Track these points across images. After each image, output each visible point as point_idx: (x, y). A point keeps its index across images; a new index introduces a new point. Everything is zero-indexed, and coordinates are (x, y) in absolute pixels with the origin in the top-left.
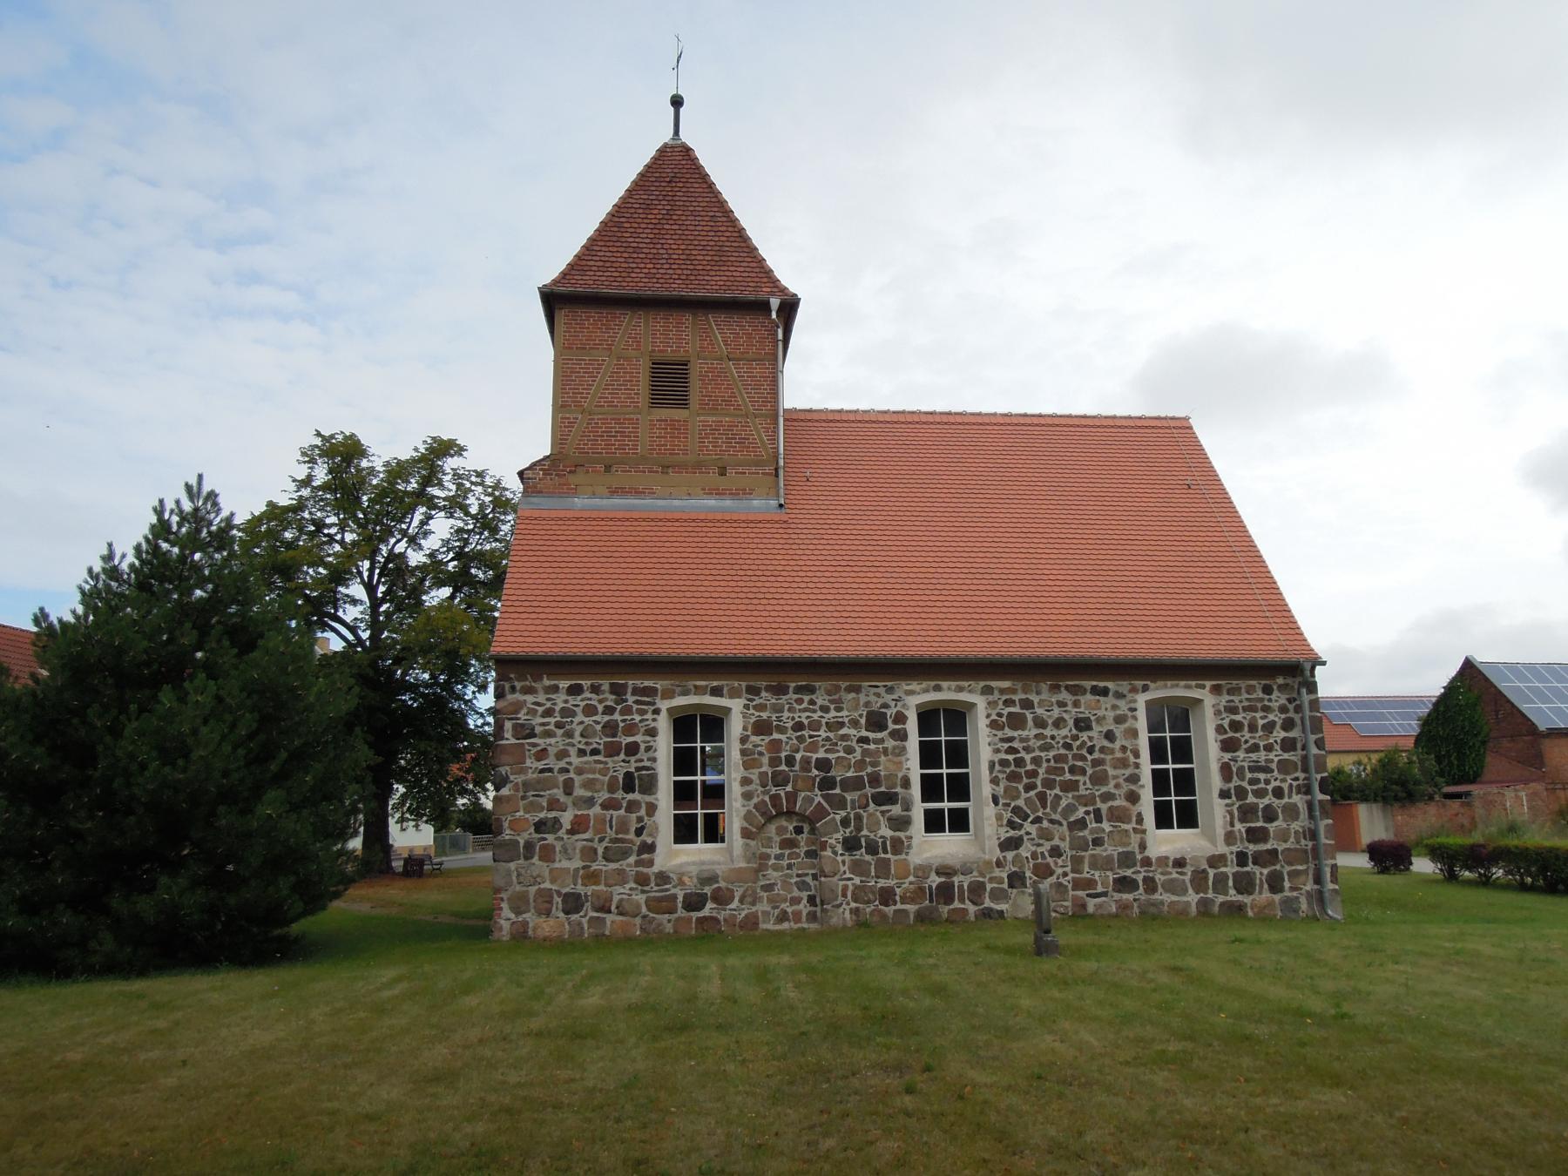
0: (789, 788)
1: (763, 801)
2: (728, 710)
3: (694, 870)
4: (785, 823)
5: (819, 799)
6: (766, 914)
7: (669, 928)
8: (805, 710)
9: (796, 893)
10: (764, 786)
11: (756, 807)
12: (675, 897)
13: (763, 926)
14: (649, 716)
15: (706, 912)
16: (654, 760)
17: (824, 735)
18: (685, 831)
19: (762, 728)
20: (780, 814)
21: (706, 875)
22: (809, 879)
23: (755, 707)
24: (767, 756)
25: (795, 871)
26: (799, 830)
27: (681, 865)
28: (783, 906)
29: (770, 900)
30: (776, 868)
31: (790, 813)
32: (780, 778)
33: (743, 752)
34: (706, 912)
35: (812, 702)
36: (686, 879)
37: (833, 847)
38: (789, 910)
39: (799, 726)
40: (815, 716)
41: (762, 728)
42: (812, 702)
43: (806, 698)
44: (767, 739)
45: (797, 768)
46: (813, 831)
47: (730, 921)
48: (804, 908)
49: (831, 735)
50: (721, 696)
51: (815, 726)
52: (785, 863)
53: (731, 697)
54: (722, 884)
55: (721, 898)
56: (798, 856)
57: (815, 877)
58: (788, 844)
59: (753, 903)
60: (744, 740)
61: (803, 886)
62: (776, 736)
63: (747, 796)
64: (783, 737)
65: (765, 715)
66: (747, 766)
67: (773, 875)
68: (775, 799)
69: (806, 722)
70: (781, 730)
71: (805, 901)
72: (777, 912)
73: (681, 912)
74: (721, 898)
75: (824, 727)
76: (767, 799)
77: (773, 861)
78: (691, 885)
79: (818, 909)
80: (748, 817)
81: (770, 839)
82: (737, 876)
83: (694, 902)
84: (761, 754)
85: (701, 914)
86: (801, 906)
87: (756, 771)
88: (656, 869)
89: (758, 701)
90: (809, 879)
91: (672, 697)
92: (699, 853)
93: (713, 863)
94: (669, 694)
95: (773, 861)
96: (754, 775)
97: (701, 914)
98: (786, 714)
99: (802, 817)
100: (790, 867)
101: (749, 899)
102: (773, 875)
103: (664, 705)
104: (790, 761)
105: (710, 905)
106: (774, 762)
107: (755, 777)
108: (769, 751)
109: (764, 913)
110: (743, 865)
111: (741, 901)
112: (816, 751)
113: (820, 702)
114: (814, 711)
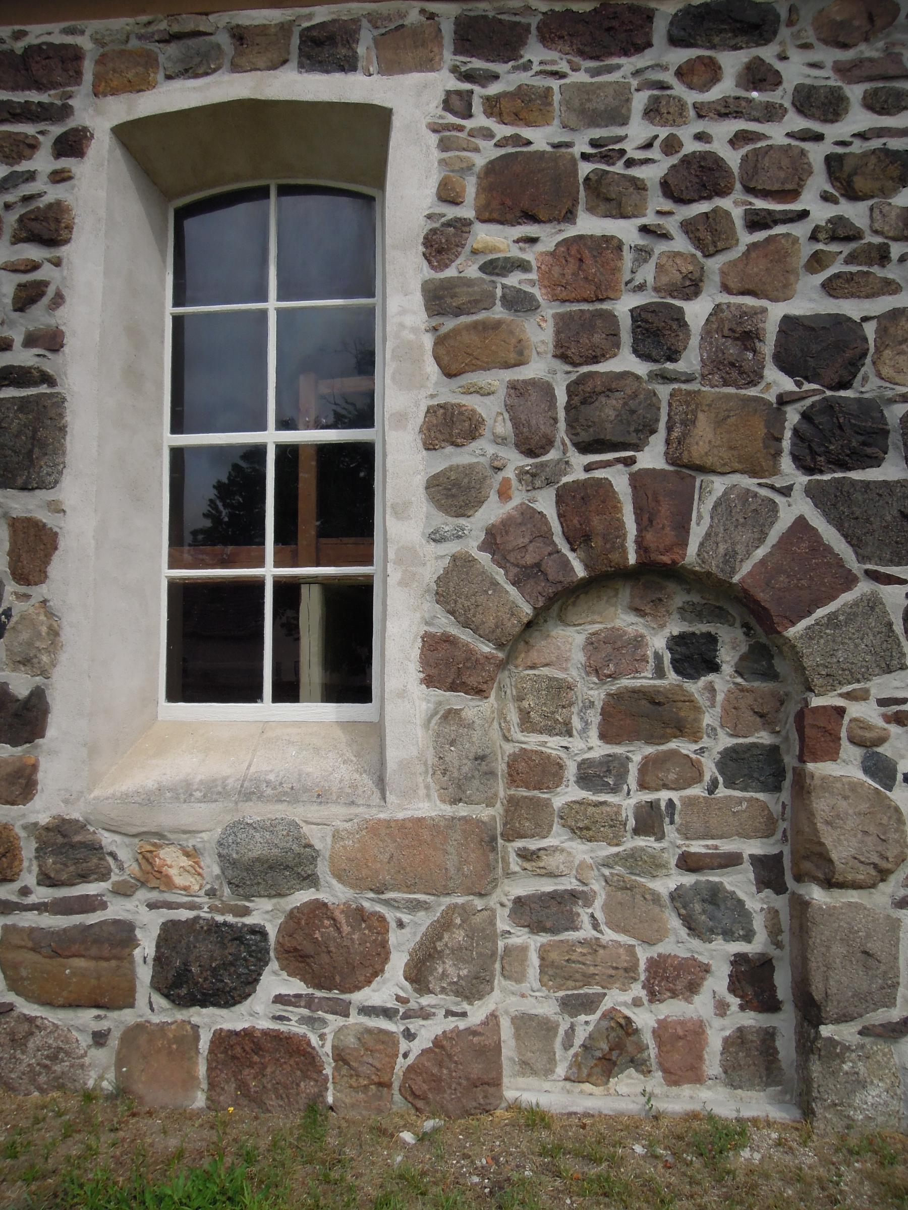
0: (652, 457)
1: (530, 517)
2: (378, 119)
3: (207, 822)
4: (626, 622)
5: (798, 507)
6: (533, 1029)
7: (99, 1070)
8: (727, 110)
9: (677, 943)
10: (532, 446)
11: (493, 541)
12: (122, 936)
13: (521, 1090)
14: (43, 162)
15: (255, 1014)
16: (52, 341)
17: (821, 213)
18: (213, 651)
19: (521, 191)
20: (605, 579)
21: (257, 847)
22: (739, 883)
23: (493, 106)
24: (550, 310)
25: (672, 842)
26: (694, 657)
27: (150, 799)
28: (617, 998)
29: (552, 972)
30: (584, 824)
31: (654, 577)
32: (608, 410)
33: (438, 299)
34: (255, 1014)
35: (759, 76)
36: (172, 860)
37: (868, 742)
38: (645, 1019)
39: (699, 177)
40: (776, 134)
41: (521, 191)
42: (759, 76)
43: (732, 62)
44: (550, 237)
45: (691, 361)
46: (762, 659)
47: (366, 1059)
48: (715, 1014)
49: (856, 213)
50: (348, 65)
51: (776, 178)
52: (628, 802)
53: (390, 68)
54: (334, 893)
55: (330, 957)
56: (691, 772)
57: (769, 873)
58: (639, 716)
59: (473, 988)
60: (440, 245)
61: (708, 912)
62: (588, 224)
63: (453, 494)
64: (625, 230)
65: (540, 138)
66: (453, 359)
67: (574, 857)
68: (584, 506)
69: (733, 158)
70: (610, 197)
71: (718, 982)
72: (586, 1025)
73: (150, 1008)
74: (330, 957)
75: (819, 181)
76: (546, 503)
77: (568, 793)
78: (194, 885)
79: (785, 1022)
80: (453, 589)
81: (559, 690)
82: (404, 856)
83: (206, 965)
84: (519, 302)
85: (233, 1019)
86: (700, 1007)
87: (497, 379)
88: (41, 809)
89: (509, 79)
90: (739, 883)
91: (140, 85)
92: (272, 745)
93: (290, 794)
94: (125, 71)
95: (568, 793)
96: (488, 398)
97: (233, 1019)
98: (637, 130)
99: (717, 595)
100: (649, 821)
101: (449, 968)
102: (574, 857)
103: (102, 117)
104: (657, 333)
105: (275, 981)
106: (580, 341)
107: (490, 409)
108: (558, 289)
109: (522, 1022)
110: (428, 807)
111: (418, 975)
112: (782, 293)
113: (795, 71)
114: (772, 113)
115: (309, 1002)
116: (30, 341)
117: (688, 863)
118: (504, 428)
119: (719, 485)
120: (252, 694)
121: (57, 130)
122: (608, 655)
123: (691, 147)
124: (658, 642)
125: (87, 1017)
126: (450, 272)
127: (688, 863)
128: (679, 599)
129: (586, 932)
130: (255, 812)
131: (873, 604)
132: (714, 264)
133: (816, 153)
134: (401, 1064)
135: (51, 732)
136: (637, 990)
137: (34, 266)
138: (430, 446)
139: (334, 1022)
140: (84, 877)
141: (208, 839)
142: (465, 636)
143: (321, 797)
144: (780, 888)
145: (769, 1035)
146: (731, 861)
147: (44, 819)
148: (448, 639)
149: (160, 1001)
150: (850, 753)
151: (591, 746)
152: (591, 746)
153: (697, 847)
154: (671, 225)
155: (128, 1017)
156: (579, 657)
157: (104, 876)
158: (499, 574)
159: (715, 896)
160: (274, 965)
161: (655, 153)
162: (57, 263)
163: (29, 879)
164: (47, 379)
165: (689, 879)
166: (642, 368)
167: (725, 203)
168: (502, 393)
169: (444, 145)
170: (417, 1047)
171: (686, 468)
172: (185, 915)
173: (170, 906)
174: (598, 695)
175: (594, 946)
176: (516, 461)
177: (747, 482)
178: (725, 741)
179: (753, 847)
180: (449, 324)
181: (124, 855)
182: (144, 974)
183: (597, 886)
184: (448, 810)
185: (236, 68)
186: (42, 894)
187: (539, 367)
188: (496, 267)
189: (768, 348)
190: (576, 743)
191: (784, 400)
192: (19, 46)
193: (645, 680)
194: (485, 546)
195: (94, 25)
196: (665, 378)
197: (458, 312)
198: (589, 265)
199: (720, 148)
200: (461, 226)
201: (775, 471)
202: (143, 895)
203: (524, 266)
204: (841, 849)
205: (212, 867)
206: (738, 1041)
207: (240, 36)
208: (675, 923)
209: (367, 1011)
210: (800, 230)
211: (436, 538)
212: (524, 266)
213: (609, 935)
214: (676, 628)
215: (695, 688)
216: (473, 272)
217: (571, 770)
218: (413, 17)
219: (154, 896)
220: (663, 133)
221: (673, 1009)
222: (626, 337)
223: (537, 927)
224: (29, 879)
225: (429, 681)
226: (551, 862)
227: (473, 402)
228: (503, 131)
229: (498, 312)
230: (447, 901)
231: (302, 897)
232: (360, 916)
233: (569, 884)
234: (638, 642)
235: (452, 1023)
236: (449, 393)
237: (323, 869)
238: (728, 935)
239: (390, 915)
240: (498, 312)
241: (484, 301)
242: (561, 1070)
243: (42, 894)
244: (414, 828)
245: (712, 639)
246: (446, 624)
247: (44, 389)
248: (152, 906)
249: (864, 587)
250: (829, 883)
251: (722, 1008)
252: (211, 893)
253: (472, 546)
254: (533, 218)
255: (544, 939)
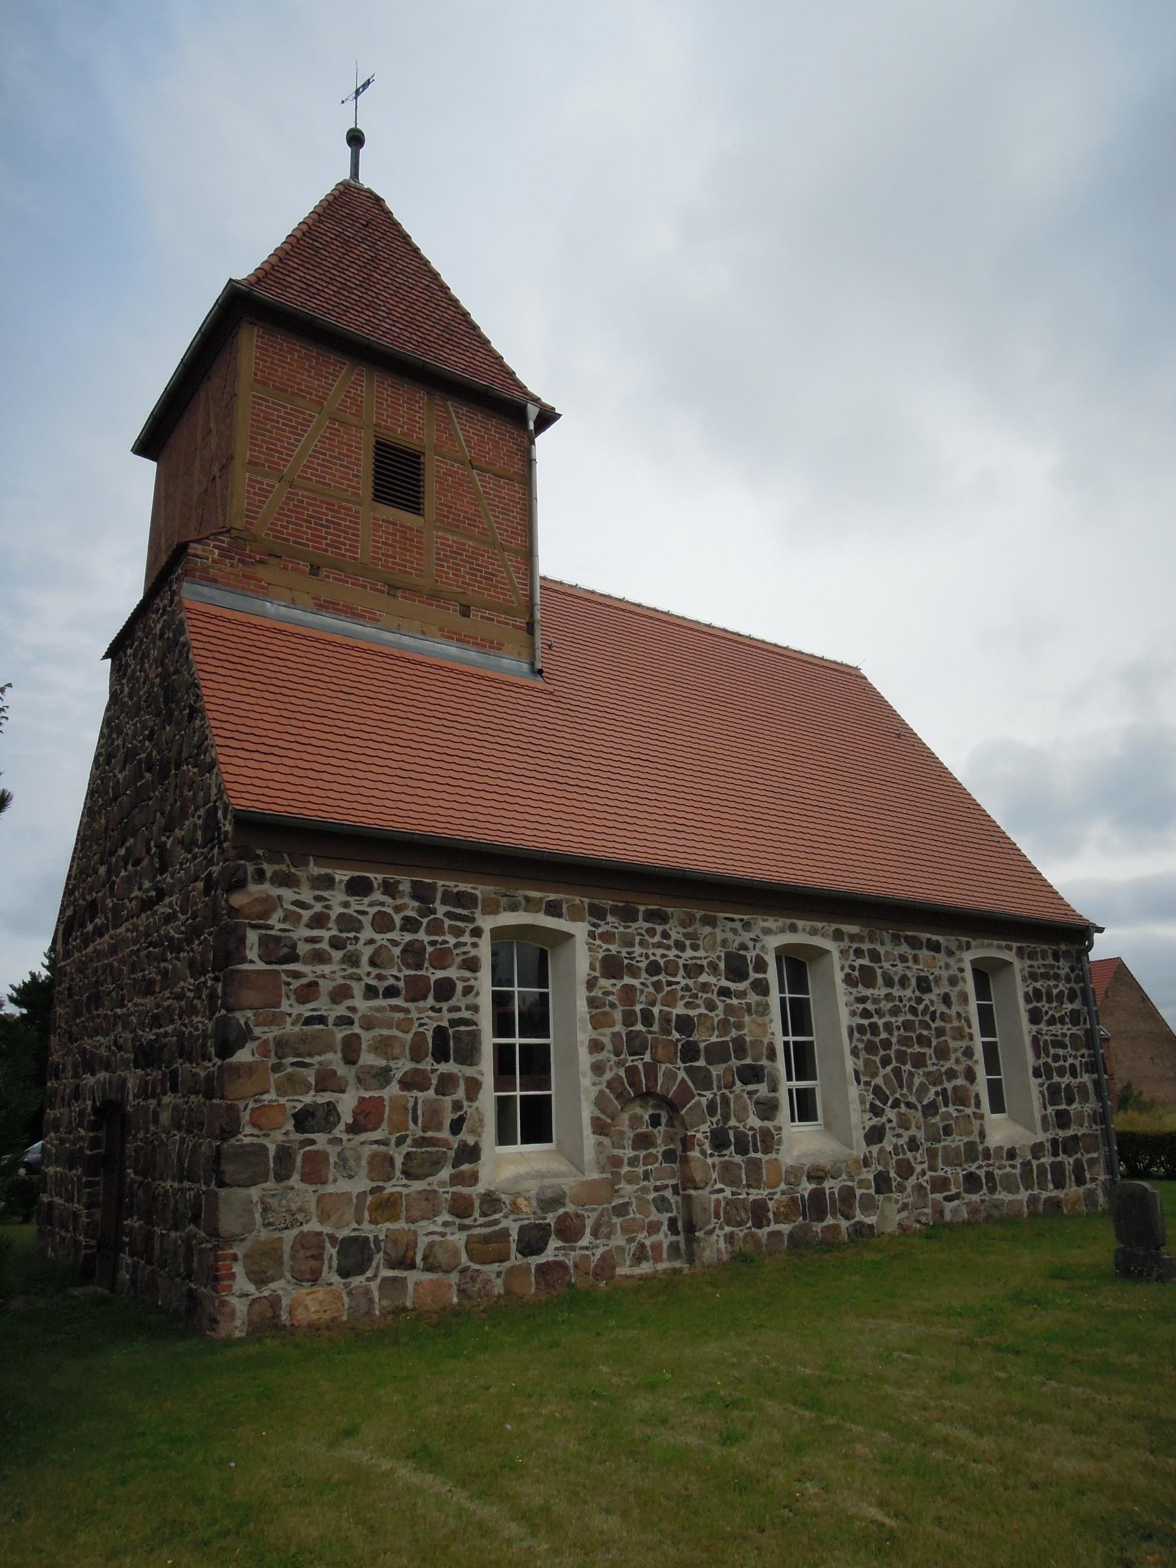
0: (647, 1058)
4: (638, 1111)
5: (682, 1074)
8: (659, 945)
9: (655, 1216)
11: (609, 1085)
12: (505, 1233)
15: (548, 1256)
17: (683, 982)
19: (612, 967)
21: (549, 1194)
22: (668, 1193)
25: (652, 1183)
26: (655, 1121)
29: (624, 1230)
33: (592, 1003)
34: (548, 1256)
36: (522, 1202)
43: (659, 929)
45: (656, 1027)
48: (664, 1237)
49: (690, 982)
52: (641, 1170)
54: (570, 1208)
55: (569, 1231)
60: (591, 984)
61: (662, 1204)
62: (628, 980)
63: (598, 1069)
69: (662, 962)
71: (665, 1228)
73: (515, 1259)
75: (681, 972)
76: (622, 1073)
79: (681, 1238)
82: (591, 1194)
83: (532, 1242)
86: (660, 1236)
87: (608, 1031)
88: (481, 1188)
90: (668, 1193)
93: (556, 1175)
94: (492, 908)
95: (625, 1169)
100: (646, 1175)
101: (604, 1230)
103: (488, 923)
104: (647, 1018)
105: (554, 1243)
107: (606, 1040)
111: (595, 1234)
113: (674, 936)
114: (668, 948)
115: (564, 1248)
116: (468, 1008)
117: (657, 1189)
118: (611, 1047)
119: (663, 1066)
120: (515, 1143)
121: (471, 926)
122: (635, 1121)
123: (652, 958)
124: (646, 1117)
125: (495, 1267)
126: (593, 994)
127: (657, 1189)
128: (651, 1103)
129: (632, 1215)
130: (547, 1182)
131: (699, 1103)
132: (659, 996)
133: (681, 962)
134: (592, 1265)
135: (483, 1158)
136: (645, 1233)
137: (468, 980)
138: (591, 1053)
139: (572, 1253)
140: (495, 1212)
141: (534, 1193)
142: (603, 1117)
143: (565, 1175)
144: (678, 1194)
145: (678, 1242)
146: (667, 1186)
147: (483, 1191)
148: (598, 1118)
149: (519, 1256)
150: (697, 1148)
151: (629, 1153)
152: (629, 1153)
153: (658, 1183)
154: (648, 983)
155: (508, 1264)
156: (627, 1122)
157: (501, 1211)
158: (612, 1096)
159: (663, 1199)
160: (553, 1237)
161: (643, 959)
162: (476, 979)
163: (476, 1214)
164: (476, 1024)
165: (656, 1194)
166: (644, 1029)
167: (660, 977)
168: (610, 1035)
169: (590, 950)
170: (598, 1256)
171: (656, 1061)
172: (527, 1222)
173: (521, 1220)
174: (631, 1135)
175: (634, 1219)
176: (614, 1058)
177: (670, 1066)
178: (664, 1148)
179: (671, 1182)
180: (594, 1011)
181: (507, 1202)
182: (514, 1246)
183: (633, 1200)
184: (601, 1176)
185: (525, 910)
186: (481, 1220)
187: (619, 1028)
188: (606, 993)
189: (673, 1024)
190: (626, 1151)
191: (678, 1040)
192: (455, 890)
193: (644, 1130)
194: (607, 1087)
195: (481, 887)
196: (650, 1032)
197: (597, 1008)
198: (628, 994)
199: (658, 958)
200: (596, 978)
201: (676, 1063)
202: (512, 1217)
203: (613, 994)
204: (698, 1177)
205: (534, 1203)
206: (671, 1245)
207: (528, 900)
208: (653, 1209)
209: (582, 1248)
210: (678, 987)
211: (594, 1084)
212: (613, 994)
213: (638, 1216)
214: (651, 1112)
215: (655, 1131)
216: (600, 995)
217: (626, 1161)
218: (577, 902)
219: (516, 1217)
220: (644, 951)
221: (654, 1238)
222: (639, 1019)
223: (618, 1216)
224: (476, 1214)
225: (594, 1133)
226: (622, 1193)
227: (602, 1038)
228: (605, 946)
229: (607, 1009)
230: (602, 1207)
231: (561, 1211)
232: (577, 1215)
233: (626, 1200)
234: (642, 1117)
235: (605, 1248)
236: (595, 1035)
237: (567, 1200)
238: (667, 1211)
239: (586, 1214)
240: (607, 1009)
241: (604, 1005)
242: (628, 1263)
243: (481, 1220)
244: (593, 1184)
245: (659, 1115)
246: (598, 1113)
247: (474, 1027)
248: (515, 1221)
249: (697, 1098)
250: (696, 1188)
251: (666, 1235)
252: (534, 1213)
253: (603, 1087)
254: (614, 978)
255: (621, 1219)
